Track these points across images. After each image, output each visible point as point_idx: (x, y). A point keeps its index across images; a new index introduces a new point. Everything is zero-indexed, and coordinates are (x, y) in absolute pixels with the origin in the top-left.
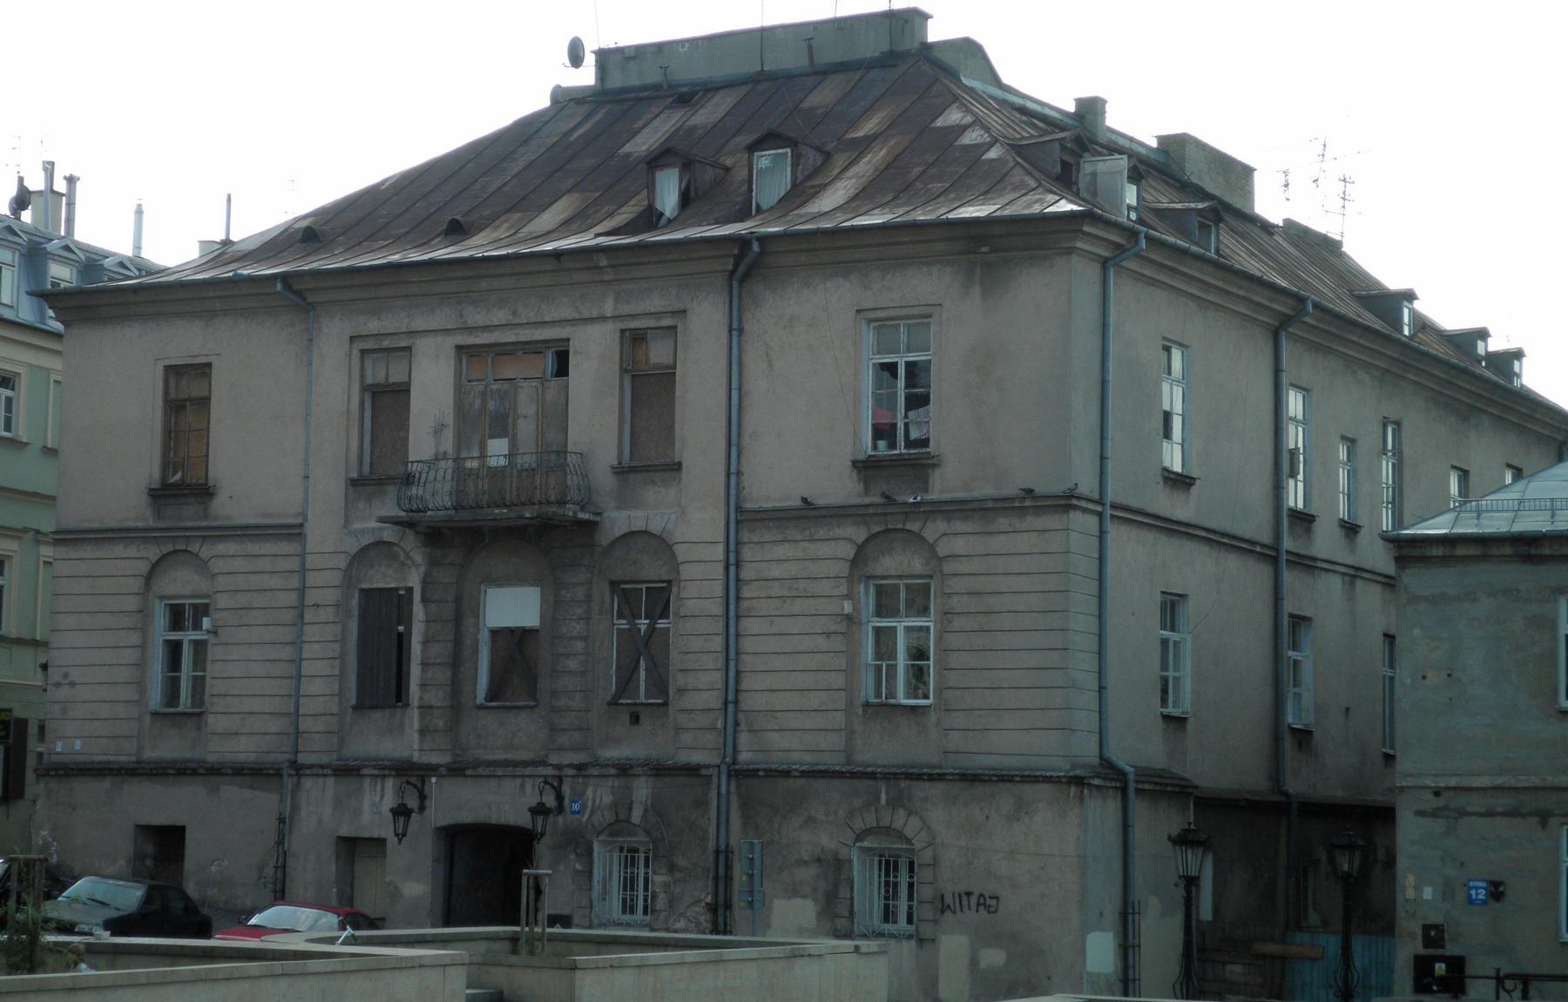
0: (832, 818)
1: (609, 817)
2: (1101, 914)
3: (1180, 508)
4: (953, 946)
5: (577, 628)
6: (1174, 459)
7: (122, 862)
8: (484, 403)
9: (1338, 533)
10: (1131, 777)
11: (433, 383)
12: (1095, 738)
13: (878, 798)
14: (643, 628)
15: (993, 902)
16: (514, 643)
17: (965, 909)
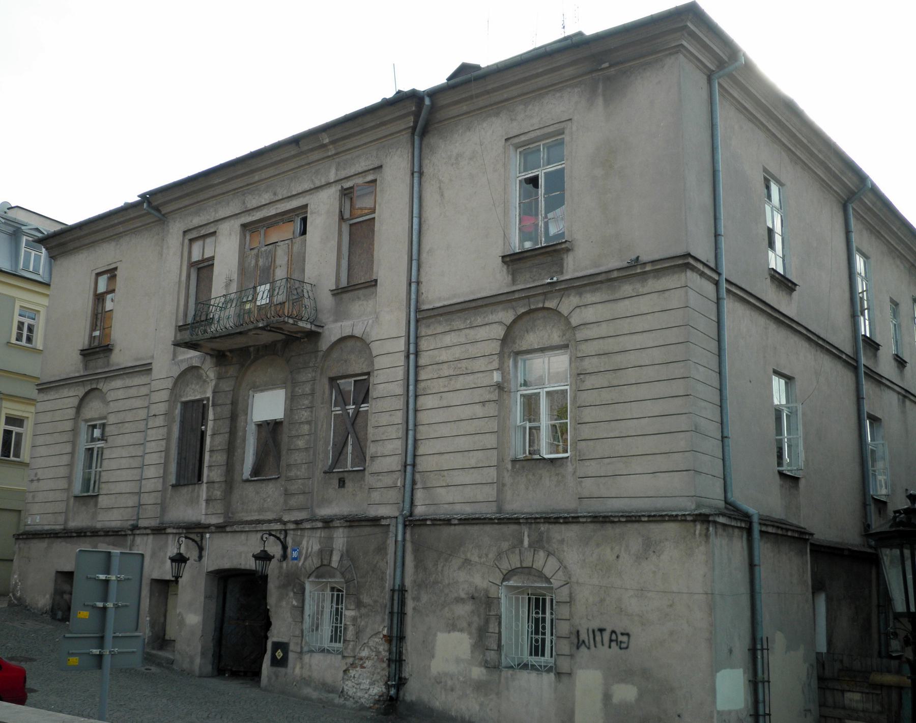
0: (483, 560)
1: (316, 562)
2: (731, 651)
3: (788, 306)
4: (588, 680)
5: (305, 415)
6: (775, 261)
7: (48, 596)
8: (257, 261)
9: (893, 363)
10: (755, 519)
11: (226, 251)
12: (720, 483)
13: (522, 542)
14: (351, 412)
15: (625, 639)
16: (271, 429)
17: (599, 645)
